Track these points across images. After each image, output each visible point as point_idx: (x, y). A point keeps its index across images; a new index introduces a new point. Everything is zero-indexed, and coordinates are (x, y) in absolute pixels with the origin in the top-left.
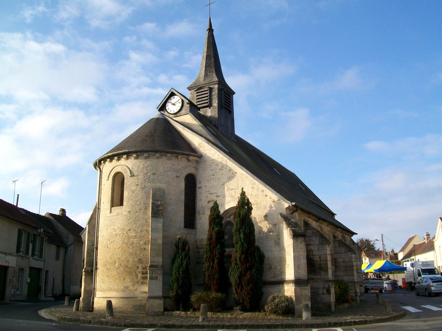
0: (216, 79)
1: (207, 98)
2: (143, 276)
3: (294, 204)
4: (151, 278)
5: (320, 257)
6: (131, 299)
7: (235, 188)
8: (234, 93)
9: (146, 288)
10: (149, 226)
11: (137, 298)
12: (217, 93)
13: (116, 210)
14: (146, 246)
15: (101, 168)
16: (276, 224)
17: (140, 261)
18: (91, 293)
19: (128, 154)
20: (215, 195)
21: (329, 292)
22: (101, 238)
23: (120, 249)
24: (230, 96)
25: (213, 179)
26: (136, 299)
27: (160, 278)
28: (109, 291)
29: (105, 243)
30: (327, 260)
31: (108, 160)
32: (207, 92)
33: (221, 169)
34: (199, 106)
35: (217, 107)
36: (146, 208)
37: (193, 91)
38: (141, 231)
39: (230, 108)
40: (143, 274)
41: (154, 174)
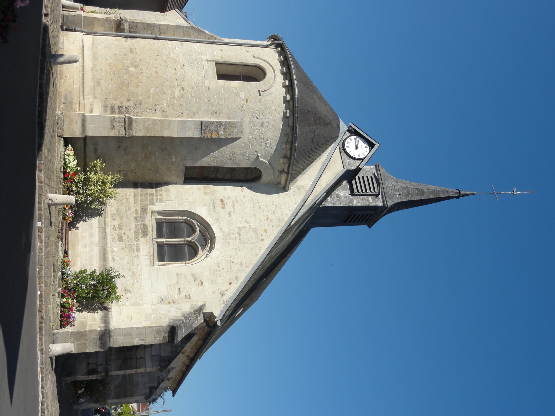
0: (390, 204)
1: (364, 190)
2: (117, 108)
3: (219, 323)
4: (112, 120)
5: (141, 358)
6: (81, 90)
7: (241, 238)
8: (370, 226)
9: (97, 112)
10: (188, 117)
11: (84, 99)
12: (371, 205)
13: (212, 71)
14: (159, 112)
15: (271, 47)
16: (190, 298)
17: (138, 104)
18: (89, 27)
19: (290, 88)
20: (232, 209)
21: (91, 372)
22: (171, 46)
23: (155, 74)
24: (366, 222)
25: (254, 207)
26: (81, 96)
28: (93, 56)
29: (164, 51)
30: (137, 368)
31: (287, 83)
32: (372, 190)
33: (268, 218)
34: (353, 182)
35: (351, 205)
36: (214, 113)
37: (375, 172)
38: (181, 105)
39: (350, 222)
40: (119, 107)
41: (262, 126)
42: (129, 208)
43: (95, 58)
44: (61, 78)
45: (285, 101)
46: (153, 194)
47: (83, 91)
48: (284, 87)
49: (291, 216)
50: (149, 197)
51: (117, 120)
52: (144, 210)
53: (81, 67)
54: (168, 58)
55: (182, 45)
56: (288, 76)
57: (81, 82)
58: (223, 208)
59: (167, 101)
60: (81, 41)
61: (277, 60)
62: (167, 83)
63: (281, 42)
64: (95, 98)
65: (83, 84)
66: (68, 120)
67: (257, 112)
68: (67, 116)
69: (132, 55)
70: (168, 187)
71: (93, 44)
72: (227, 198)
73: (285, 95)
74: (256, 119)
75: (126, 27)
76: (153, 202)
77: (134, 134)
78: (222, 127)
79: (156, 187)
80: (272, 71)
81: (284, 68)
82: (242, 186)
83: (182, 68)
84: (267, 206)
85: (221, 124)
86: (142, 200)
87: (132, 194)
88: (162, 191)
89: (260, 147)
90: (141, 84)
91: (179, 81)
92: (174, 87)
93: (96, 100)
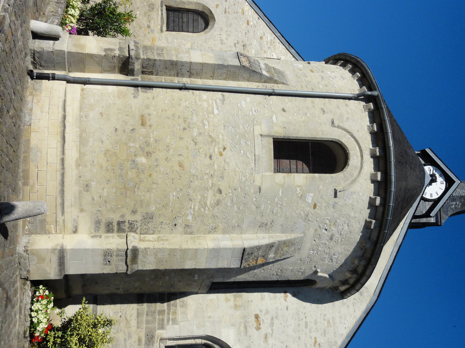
2: (115, 224)
6: (59, 201)
11: (63, 213)
13: (266, 151)
20: (269, 331)
23: (177, 168)
25: (299, 325)
27: (107, 270)
28: (81, 136)
33: (316, 342)
36: (264, 226)
41: (331, 239)
42: (130, 336)
43: (82, 141)
44: (26, 184)
45: (371, 204)
46: (164, 311)
47: (63, 204)
48: (373, 181)
49: (347, 337)
50: (157, 317)
51: (115, 253)
52: (150, 338)
53: (59, 162)
54: (200, 134)
55: (223, 100)
56: (382, 164)
57: (59, 188)
58: (258, 328)
59: (194, 211)
60: (61, 104)
61: (366, 128)
62: (196, 183)
63: (375, 93)
64: (82, 210)
65: (62, 192)
66: (36, 258)
67: (328, 222)
68: (33, 254)
69: (143, 130)
70: (185, 299)
71: (81, 109)
72: (264, 312)
73: (372, 196)
74: (324, 231)
75: (137, 66)
76: (163, 324)
77: (140, 268)
78: (274, 249)
79: (169, 300)
80: (359, 154)
81: (377, 149)
82: (285, 292)
83: (221, 155)
84: (316, 323)
85: (273, 246)
86: (147, 322)
87: (135, 313)
88: (176, 306)
89: (322, 262)
90: (154, 186)
91: (215, 179)
92: (207, 189)
93: (83, 214)
